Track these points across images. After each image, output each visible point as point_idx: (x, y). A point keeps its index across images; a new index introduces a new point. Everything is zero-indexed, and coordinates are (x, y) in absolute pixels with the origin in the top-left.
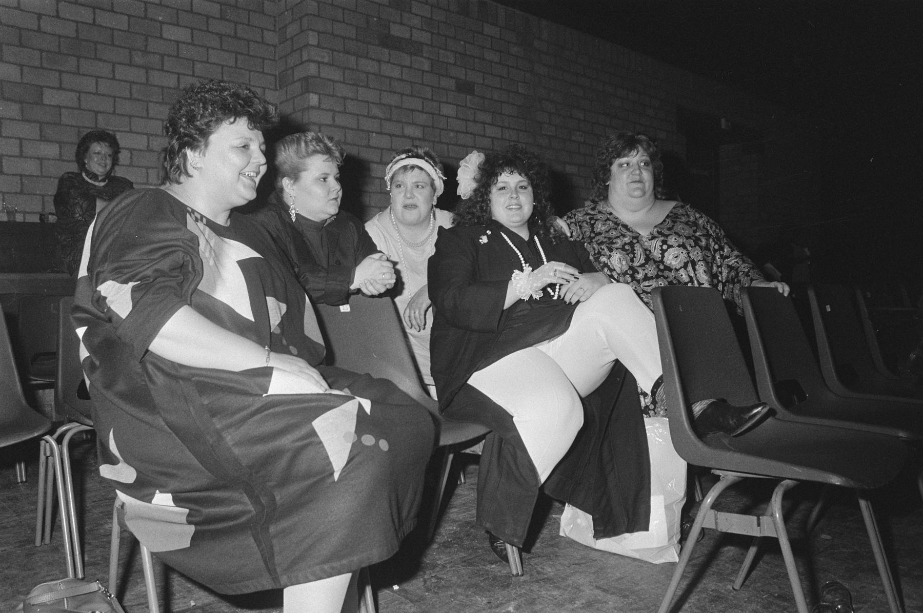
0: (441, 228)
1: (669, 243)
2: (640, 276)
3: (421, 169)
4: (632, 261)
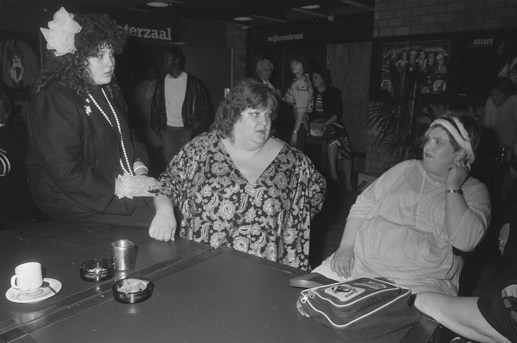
0: (122, 175)
1: (214, 228)
2: (240, 222)
4: (288, 183)
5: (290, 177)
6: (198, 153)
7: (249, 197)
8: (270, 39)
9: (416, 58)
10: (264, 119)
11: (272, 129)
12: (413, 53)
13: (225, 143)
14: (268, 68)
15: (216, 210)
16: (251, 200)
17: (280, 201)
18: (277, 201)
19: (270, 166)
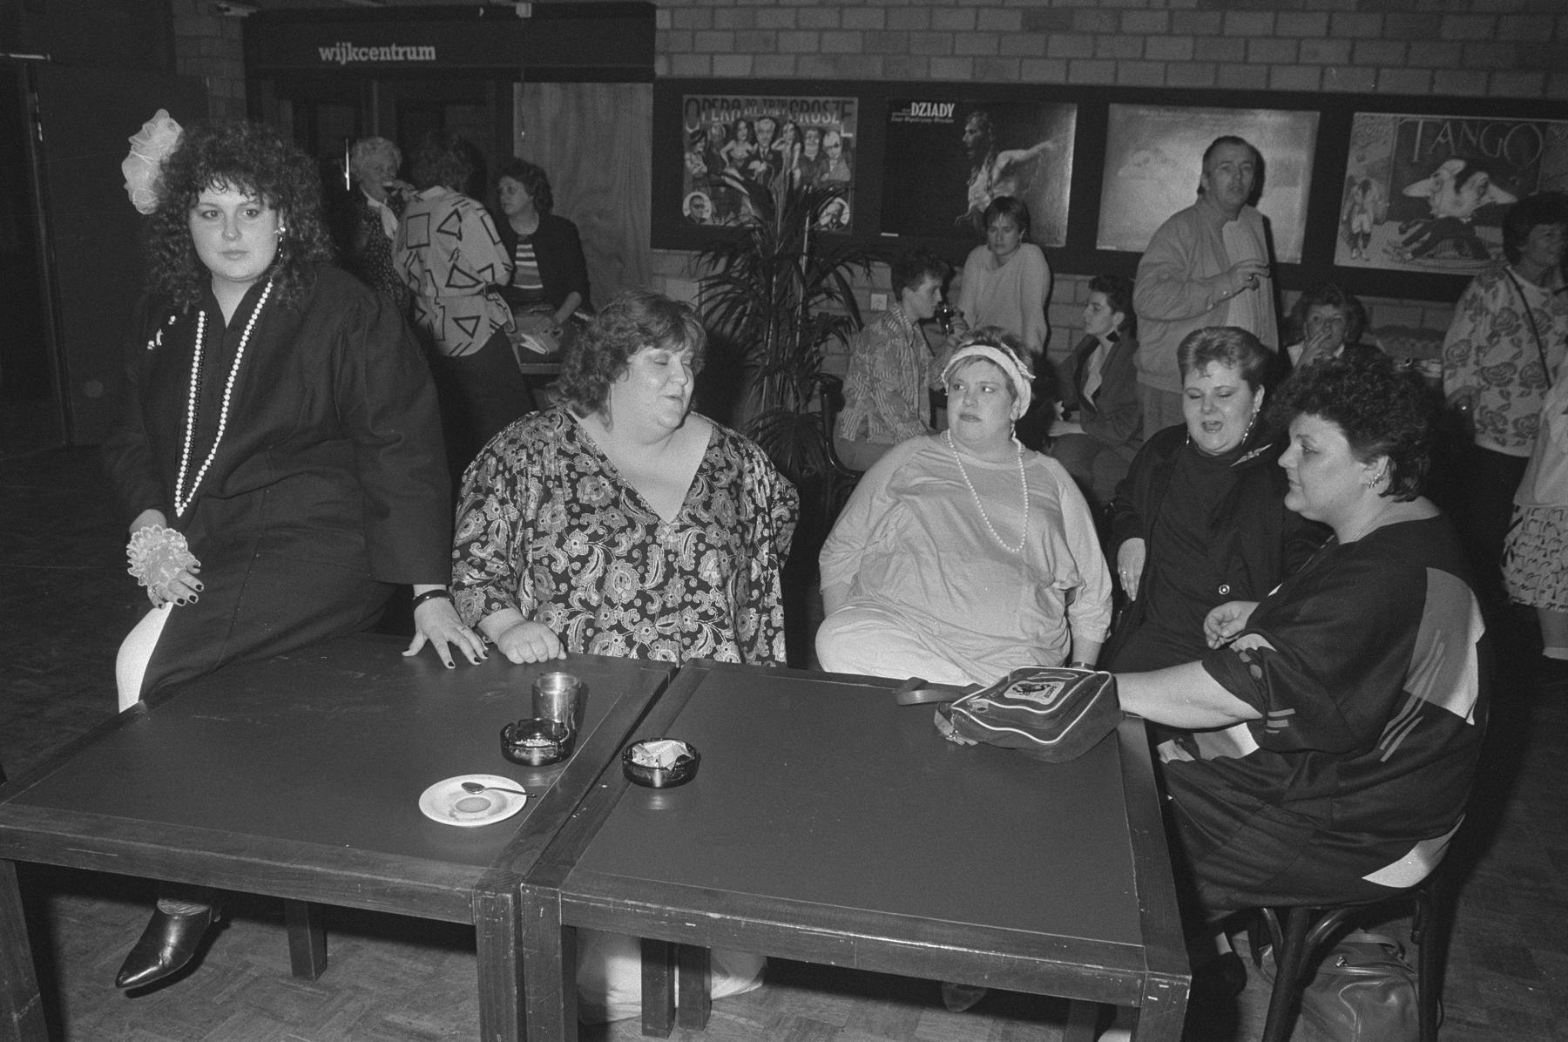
2: (654, 608)
3: (992, 362)
4: (643, 579)
5: (738, 498)
6: (536, 457)
7: (667, 552)
8: (326, 54)
9: (773, 140)
10: (680, 368)
11: (694, 393)
12: (766, 126)
13: (590, 426)
14: (387, 164)
15: (600, 584)
16: (671, 558)
17: (730, 552)
18: (724, 554)
19: (696, 480)
